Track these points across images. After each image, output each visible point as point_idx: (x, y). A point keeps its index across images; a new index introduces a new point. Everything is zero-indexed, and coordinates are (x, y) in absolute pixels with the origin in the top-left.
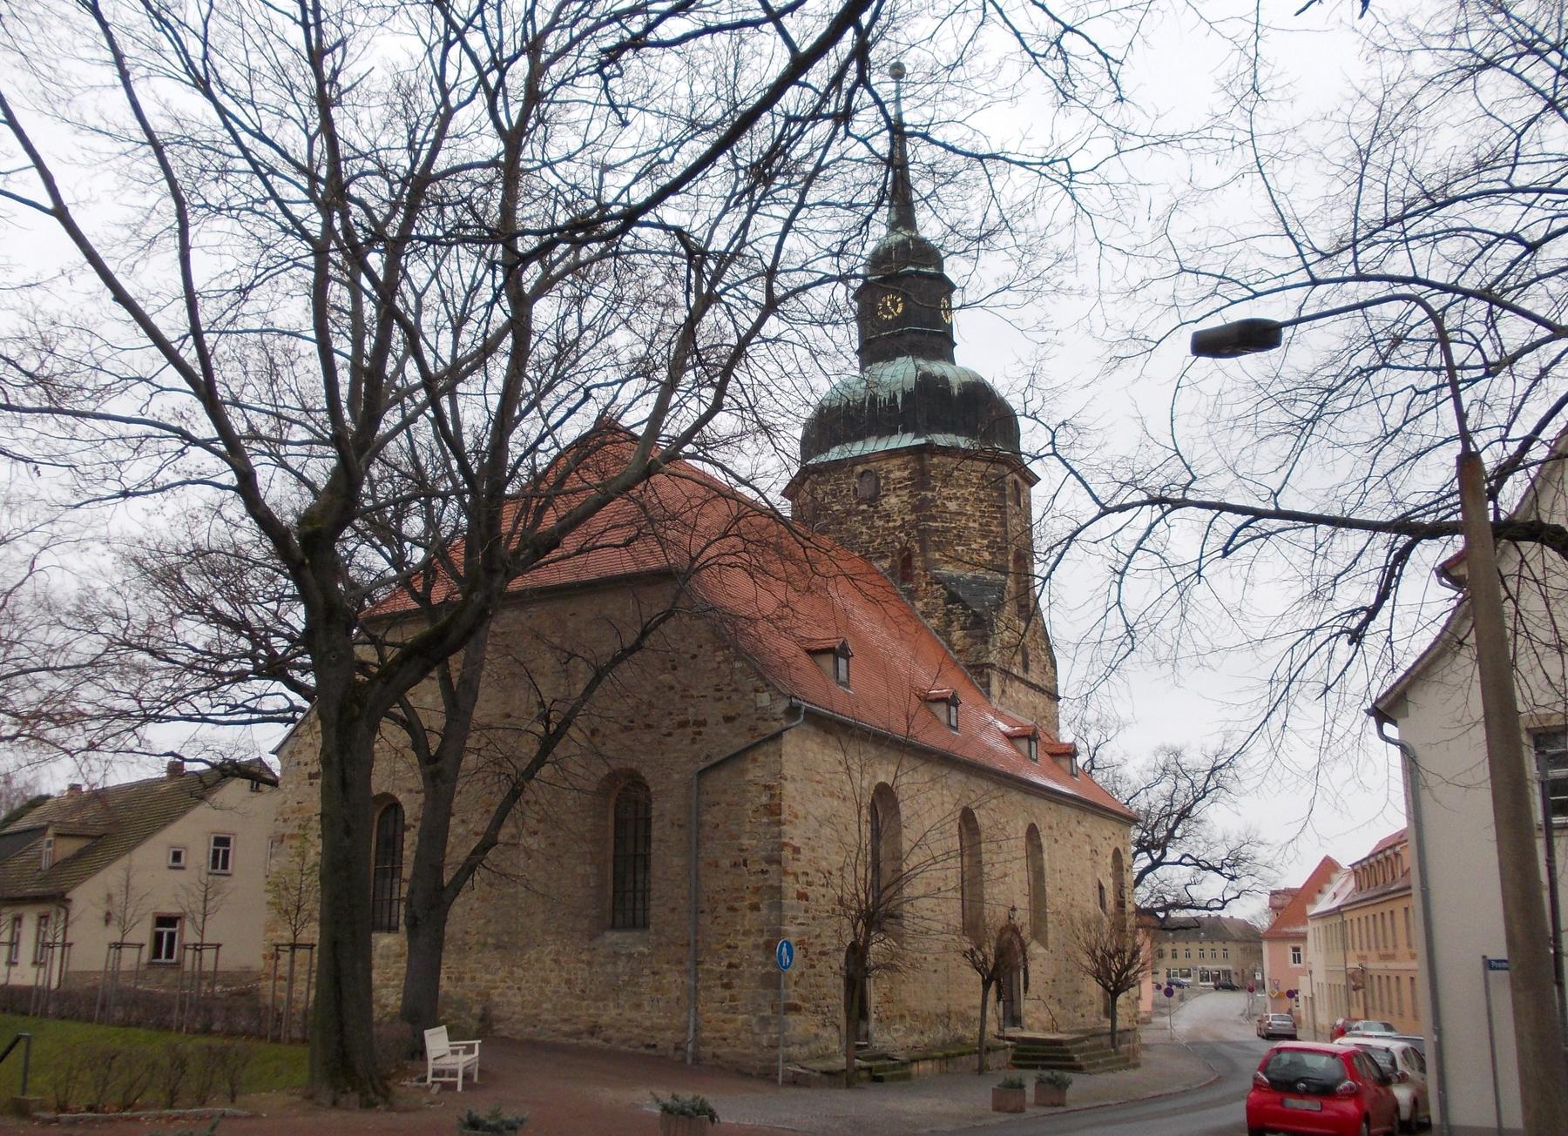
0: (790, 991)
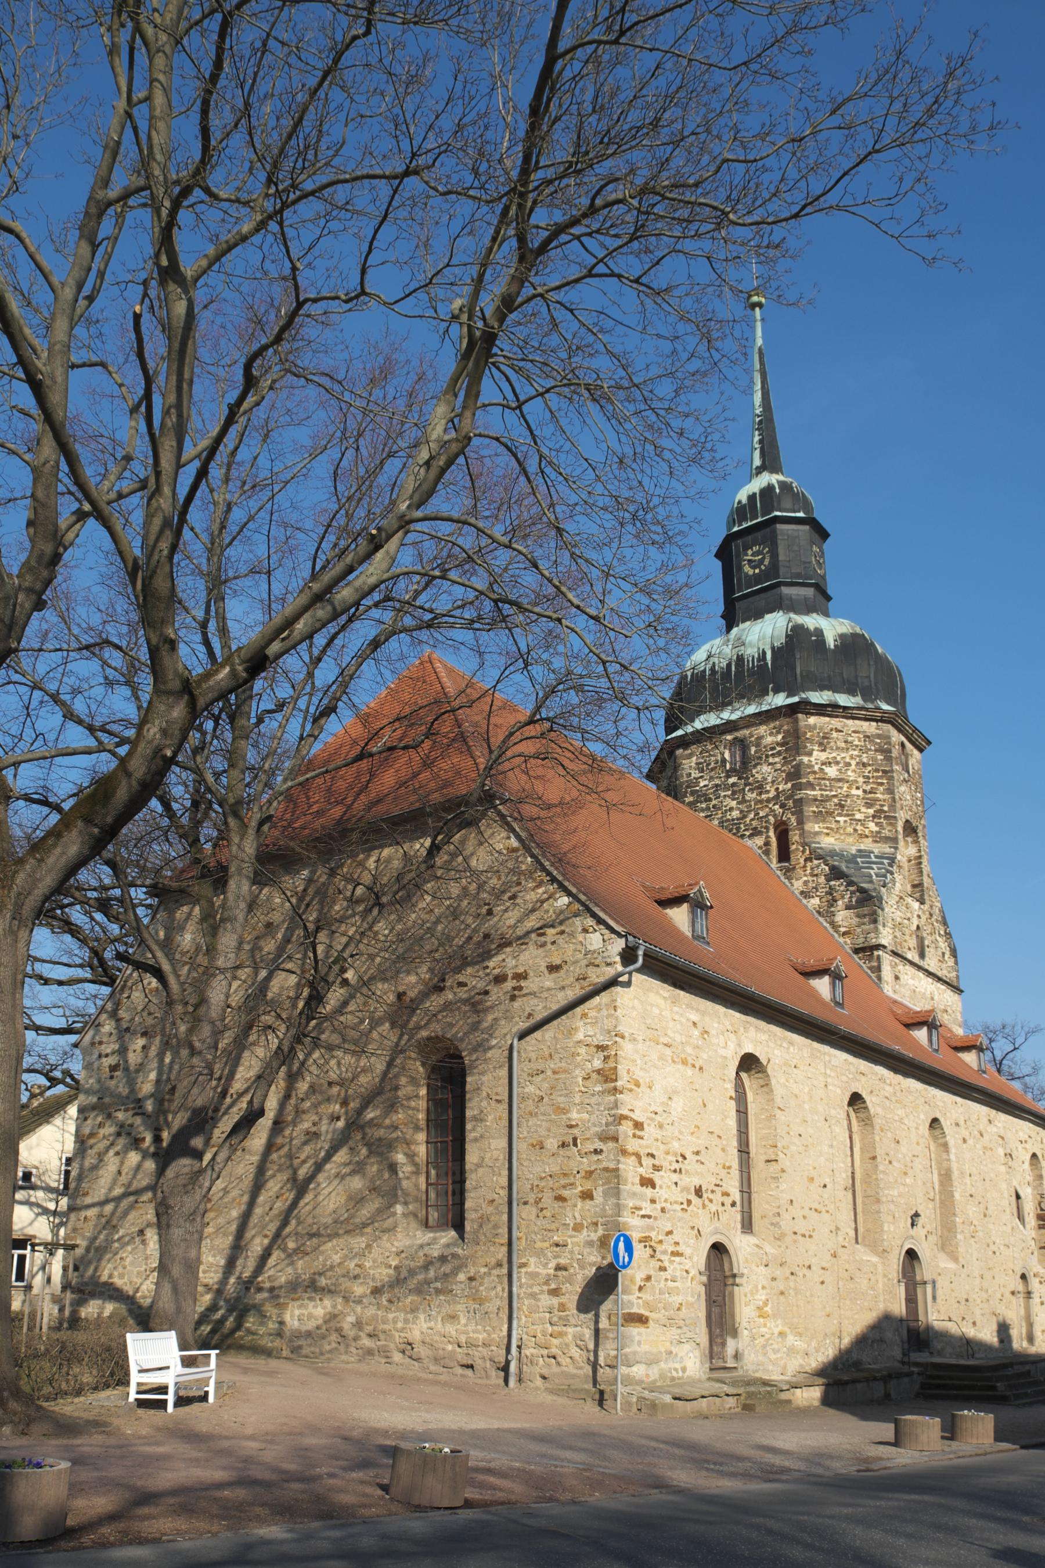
0: (632, 1298)
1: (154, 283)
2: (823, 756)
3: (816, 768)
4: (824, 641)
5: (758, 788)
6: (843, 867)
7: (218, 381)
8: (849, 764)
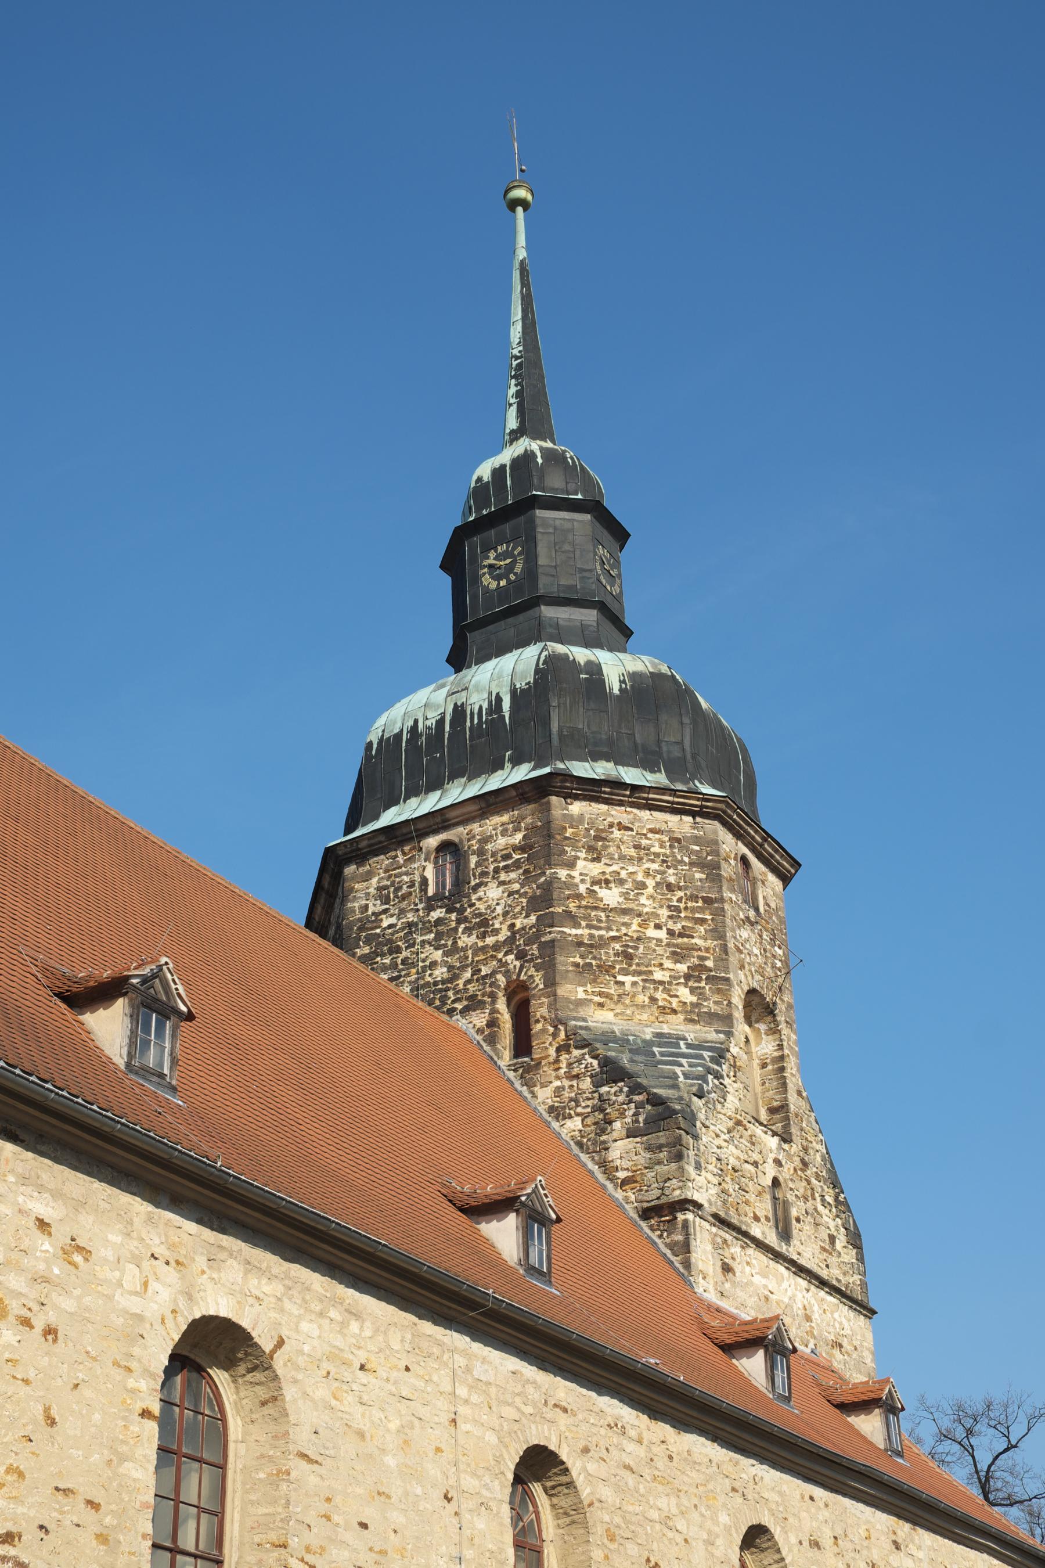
2: (595, 869)
3: (582, 889)
4: (601, 682)
5: (481, 924)
6: (625, 1060)
8: (643, 886)
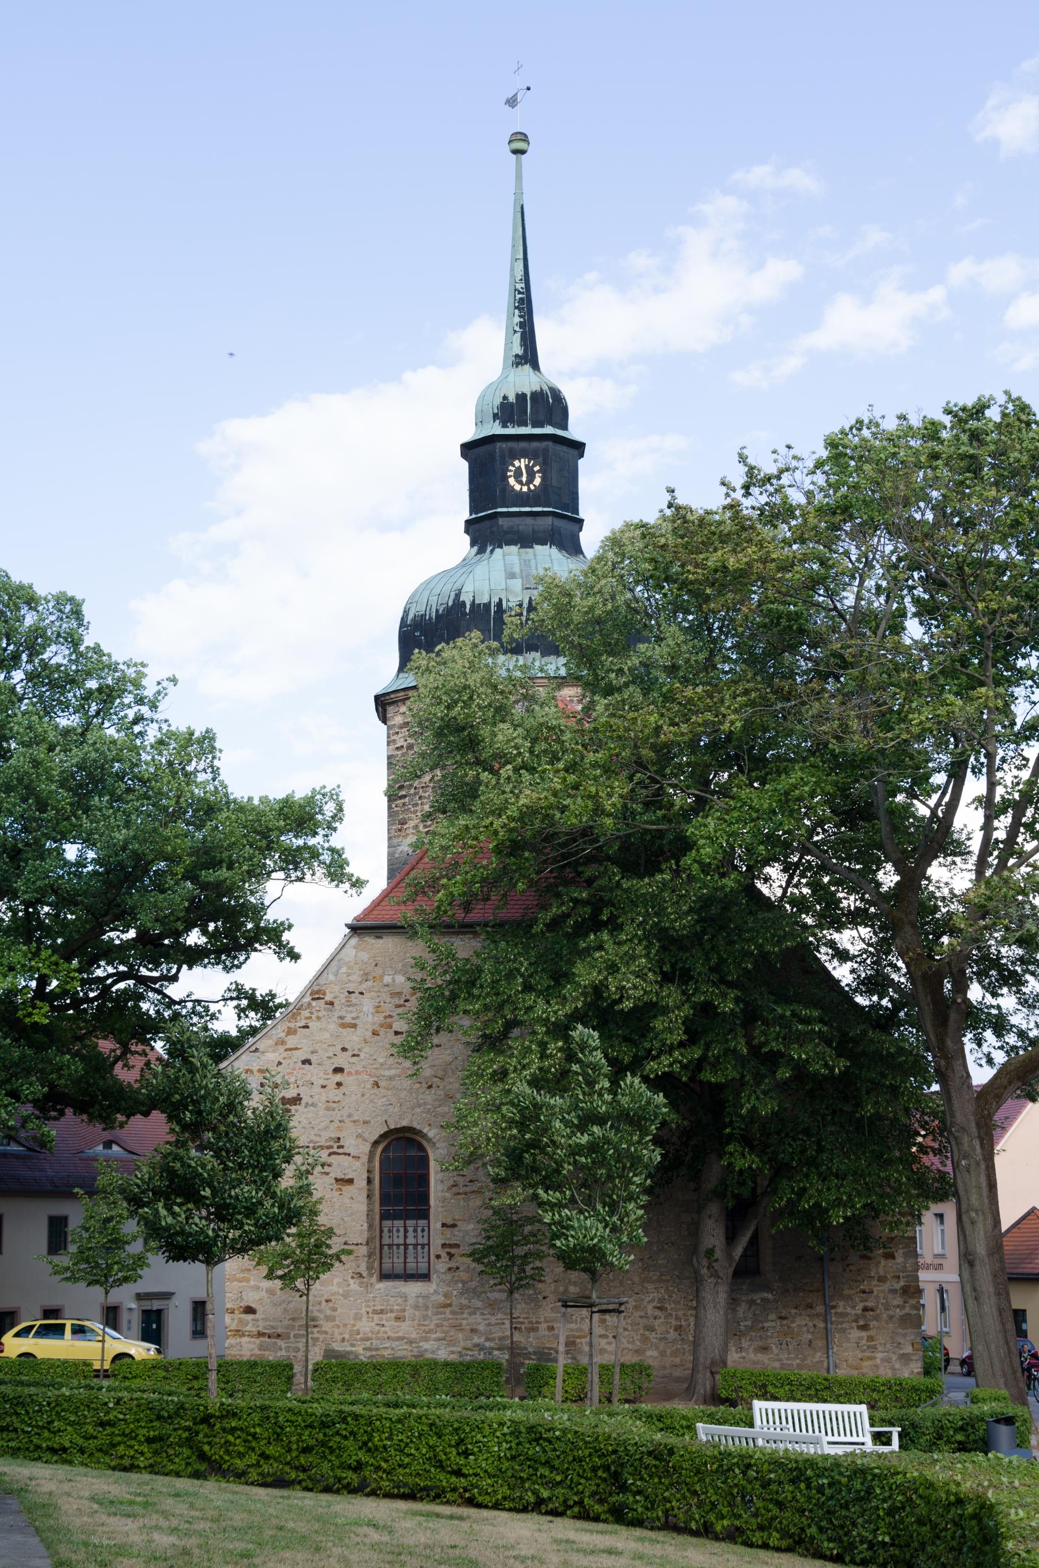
1: (386, 1538)
7: (547, 1462)
